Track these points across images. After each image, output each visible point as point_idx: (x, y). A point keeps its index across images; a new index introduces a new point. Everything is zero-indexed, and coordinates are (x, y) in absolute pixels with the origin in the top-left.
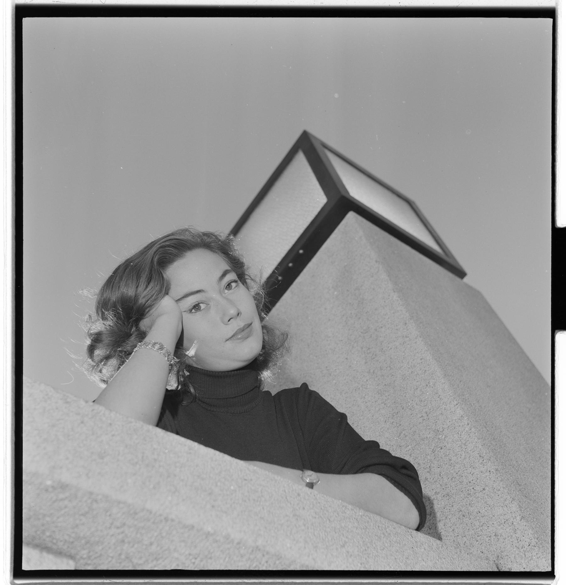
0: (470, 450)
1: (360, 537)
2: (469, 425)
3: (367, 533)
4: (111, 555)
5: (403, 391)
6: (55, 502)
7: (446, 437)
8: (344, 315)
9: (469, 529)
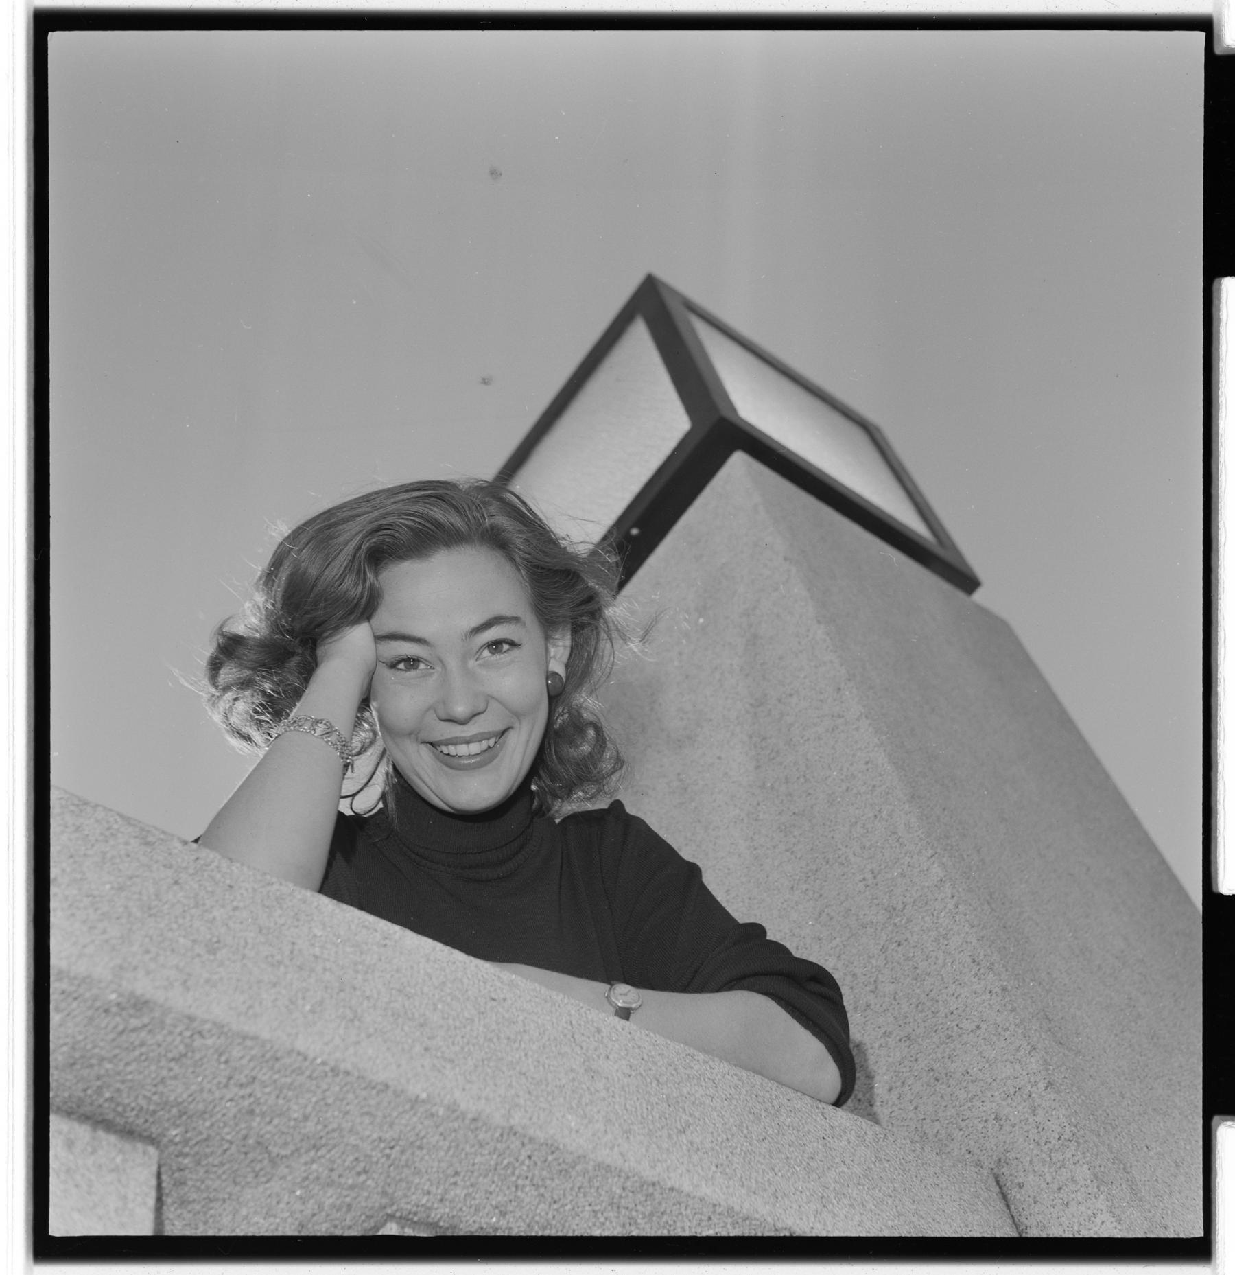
0: (954, 948)
1: (718, 1116)
2: (955, 898)
3: (732, 1107)
6: (122, 1032)
7: (909, 921)
8: (716, 668)
9: (946, 1106)
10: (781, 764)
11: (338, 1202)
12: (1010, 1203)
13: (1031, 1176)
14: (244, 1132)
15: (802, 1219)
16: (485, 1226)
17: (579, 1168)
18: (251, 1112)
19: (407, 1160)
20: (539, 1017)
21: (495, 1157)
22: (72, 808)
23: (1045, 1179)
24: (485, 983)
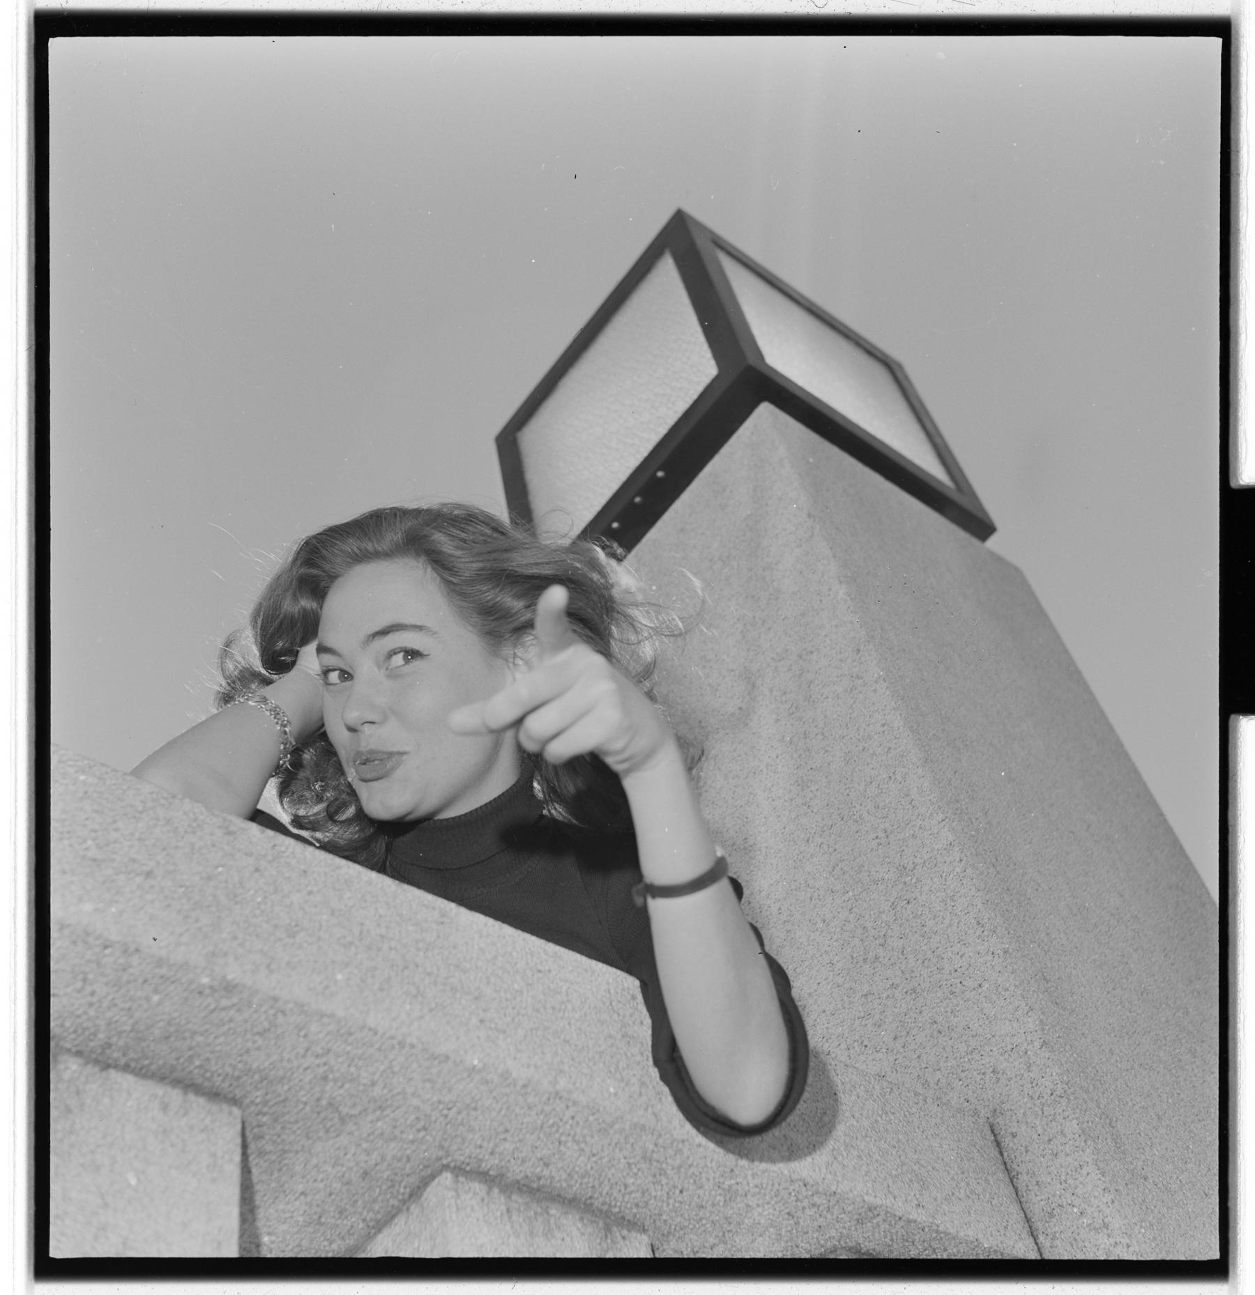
4: (304, 1099)
5: (845, 785)
6: (214, 1010)
7: (918, 880)
9: (947, 1057)
10: (800, 719)
11: (399, 1154)
12: (1003, 1150)
13: (1024, 1128)
14: (317, 1095)
15: (814, 1171)
16: (530, 1175)
17: (617, 1127)
18: (325, 1078)
19: (463, 1120)
20: (580, 987)
21: (542, 1117)
22: (163, 801)
23: (1036, 1131)
24: (532, 956)
